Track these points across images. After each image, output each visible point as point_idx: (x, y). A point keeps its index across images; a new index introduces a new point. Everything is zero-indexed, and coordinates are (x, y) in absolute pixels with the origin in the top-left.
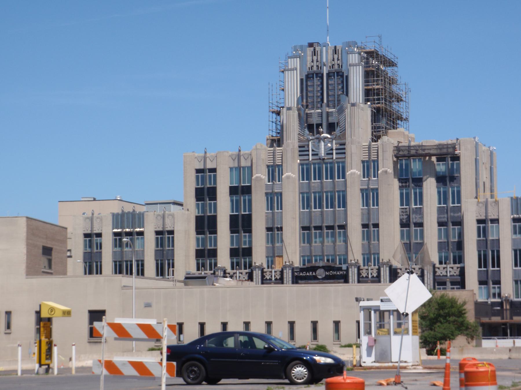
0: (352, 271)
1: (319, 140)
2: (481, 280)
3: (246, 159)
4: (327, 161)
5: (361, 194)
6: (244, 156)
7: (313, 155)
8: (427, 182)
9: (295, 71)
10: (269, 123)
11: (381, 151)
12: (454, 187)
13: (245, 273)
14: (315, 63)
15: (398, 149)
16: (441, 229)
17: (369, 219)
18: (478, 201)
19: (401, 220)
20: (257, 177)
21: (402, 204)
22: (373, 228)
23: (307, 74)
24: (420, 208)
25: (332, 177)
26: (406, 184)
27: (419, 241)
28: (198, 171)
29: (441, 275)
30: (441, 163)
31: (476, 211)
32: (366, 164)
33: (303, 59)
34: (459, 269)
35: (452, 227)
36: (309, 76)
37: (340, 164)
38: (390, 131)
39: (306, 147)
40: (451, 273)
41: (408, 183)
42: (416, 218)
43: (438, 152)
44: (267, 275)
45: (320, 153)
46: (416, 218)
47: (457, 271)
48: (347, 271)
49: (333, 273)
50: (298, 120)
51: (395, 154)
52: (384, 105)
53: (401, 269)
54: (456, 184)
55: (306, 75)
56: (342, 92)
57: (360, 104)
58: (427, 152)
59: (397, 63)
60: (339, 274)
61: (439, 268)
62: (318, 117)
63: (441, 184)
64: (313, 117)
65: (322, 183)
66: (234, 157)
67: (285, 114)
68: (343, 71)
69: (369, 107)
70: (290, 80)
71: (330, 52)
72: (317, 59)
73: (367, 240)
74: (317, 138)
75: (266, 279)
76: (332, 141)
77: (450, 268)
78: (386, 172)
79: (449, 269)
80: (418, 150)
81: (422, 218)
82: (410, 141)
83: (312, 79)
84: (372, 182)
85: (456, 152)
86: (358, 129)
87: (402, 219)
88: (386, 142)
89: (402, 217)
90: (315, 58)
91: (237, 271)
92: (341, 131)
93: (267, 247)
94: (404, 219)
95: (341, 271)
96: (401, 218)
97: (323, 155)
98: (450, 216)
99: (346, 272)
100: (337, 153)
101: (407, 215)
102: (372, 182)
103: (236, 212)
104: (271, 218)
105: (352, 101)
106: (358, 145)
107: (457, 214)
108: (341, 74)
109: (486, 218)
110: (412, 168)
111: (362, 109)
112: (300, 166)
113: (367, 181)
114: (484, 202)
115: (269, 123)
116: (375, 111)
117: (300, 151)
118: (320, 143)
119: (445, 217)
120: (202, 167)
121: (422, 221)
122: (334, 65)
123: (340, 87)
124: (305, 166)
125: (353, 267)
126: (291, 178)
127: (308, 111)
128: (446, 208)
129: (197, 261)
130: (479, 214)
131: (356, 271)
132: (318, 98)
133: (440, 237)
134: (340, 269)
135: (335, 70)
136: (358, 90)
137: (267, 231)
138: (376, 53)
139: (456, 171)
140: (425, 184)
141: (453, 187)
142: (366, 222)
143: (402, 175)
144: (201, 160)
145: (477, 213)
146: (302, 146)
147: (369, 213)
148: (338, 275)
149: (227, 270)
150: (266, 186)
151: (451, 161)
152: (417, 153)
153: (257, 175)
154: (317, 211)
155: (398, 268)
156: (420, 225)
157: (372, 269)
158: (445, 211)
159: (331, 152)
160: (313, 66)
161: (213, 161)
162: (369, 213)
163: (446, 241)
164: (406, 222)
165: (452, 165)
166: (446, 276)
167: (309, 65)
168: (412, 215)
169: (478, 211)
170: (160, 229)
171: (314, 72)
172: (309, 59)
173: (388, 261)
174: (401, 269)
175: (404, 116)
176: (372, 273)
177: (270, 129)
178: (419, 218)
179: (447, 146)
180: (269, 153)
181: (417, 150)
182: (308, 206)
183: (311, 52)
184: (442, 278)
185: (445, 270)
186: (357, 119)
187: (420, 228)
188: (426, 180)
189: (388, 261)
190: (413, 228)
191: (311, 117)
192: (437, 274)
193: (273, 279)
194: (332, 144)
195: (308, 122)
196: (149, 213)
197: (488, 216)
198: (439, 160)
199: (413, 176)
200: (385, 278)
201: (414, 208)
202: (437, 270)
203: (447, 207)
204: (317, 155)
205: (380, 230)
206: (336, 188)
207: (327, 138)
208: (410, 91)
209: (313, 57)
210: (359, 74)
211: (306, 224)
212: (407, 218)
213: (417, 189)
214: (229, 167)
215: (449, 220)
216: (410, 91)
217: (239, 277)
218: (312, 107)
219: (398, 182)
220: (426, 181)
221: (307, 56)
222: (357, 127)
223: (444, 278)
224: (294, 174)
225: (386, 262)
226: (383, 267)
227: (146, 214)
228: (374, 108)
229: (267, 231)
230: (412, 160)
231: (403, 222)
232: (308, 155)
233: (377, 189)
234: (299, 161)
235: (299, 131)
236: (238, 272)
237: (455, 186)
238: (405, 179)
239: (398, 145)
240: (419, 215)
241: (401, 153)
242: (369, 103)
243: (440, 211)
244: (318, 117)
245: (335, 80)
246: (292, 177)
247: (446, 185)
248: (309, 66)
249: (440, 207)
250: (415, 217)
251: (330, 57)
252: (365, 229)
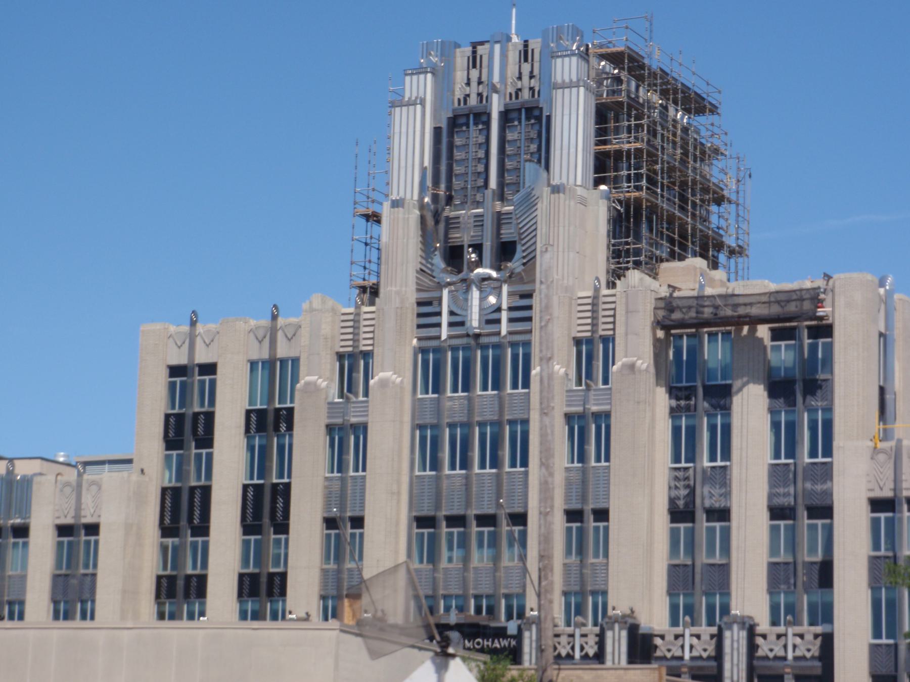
1: (467, 283)
2: (879, 673)
3: (290, 338)
4: (484, 340)
5: (567, 427)
6: (286, 331)
7: (451, 325)
8: (742, 395)
9: (419, 107)
10: (352, 246)
11: (624, 312)
12: (816, 410)
13: (708, 638)
14: (474, 89)
15: (668, 304)
16: (172, 455)
17: (584, 498)
18: (875, 448)
19: (672, 501)
20: (308, 384)
21: (676, 458)
22: (596, 520)
23: (451, 115)
24: (724, 468)
25: (498, 385)
26: (687, 402)
27: (718, 559)
28: (176, 371)
29: (771, 655)
30: (783, 344)
31: (868, 475)
32: (584, 347)
33: (443, 77)
34: (820, 639)
35: (806, 522)
36: (456, 123)
37: (519, 350)
38: (664, 265)
39: (435, 303)
40: (694, 650)
41: (693, 399)
42: (711, 496)
43: (775, 310)
44: (562, 644)
45: (469, 319)
46: (711, 496)
47: (814, 645)
48: (519, 637)
49: (483, 643)
50: (420, 233)
51: (659, 319)
52: (643, 194)
53: (662, 637)
54: (821, 401)
55: (449, 118)
56: (408, 101)
57: (577, 188)
58: (742, 311)
59: (717, 105)
60: (498, 646)
61: (764, 636)
62: (475, 226)
63: (782, 400)
64: (462, 226)
65: (470, 400)
66: (260, 334)
67: (387, 217)
68: (540, 106)
69: (602, 198)
70: (404, 130)
71: (513, 56)
72: (480, 78)
73: (489, 546)
74: (464, 280)
76: (500, 288)
77: (795, 635)
78: (632, 367)
79: (791, 640)
80: (720, 306)
81: (727, 495)
82: (702, 287)
83: (464, 128)
84: (595, 395)
85: (819, 310)
86: (566, 254)
87: (675, 498)
88: (634, 287)
89: (674, 493)
90: (474, 74)
91: (787, 630)
92: (525, 261)
93: (324, 572)
94: (679, 498)
95: (503, 639)
96: (673, 495)
97: (475, 323)
98: (804, 490)
99: (517, 643)
100: (511, 320)
101: (688, 486)
102: (595, 395)
103: (258, 479)
104: (339, 492)
105: (556, 181)
106: (564, 296)
107: (822, 486)
108: (536, 113)
109: (895, 496)
110: (706, 357)
111: (583, 202)
112: (420, 356)
113: (583, 393)
114: (891, 450)
115: (352, 246)
116: (622, 210)
117: (420, 315)
118: (470, 293)
119: (788, 494)
120: (183, 360)
121: (728, 505)
122: (520, 90)
123: (533, 147)
124: (431, 355)
125: (735, 627)
126: (391, 385)
127: (448, 212)
128: (792, 468)
129: (158, 608)
130: (876, 483)
132: (478, 177)
133: (774, 549)
134: (501, 633)
135: (523, 103)
136: (572, 150)
137: (328, 528)
138: (683, 92)
139: (823, 365)
140: (737, 401)
141: (812, 411)
142: (575, 506)
143: (679, 379)
144: (184, 343)
145: (869, 482)
146: (425, 300)
147: (584, 482)
148: (496, 648)
149: (758, 625)
150: (329, 408)
151: (809, 338)
152: (716, 314)
153: (308, 378)
154: (454, 476)
155: (656, 633)
156: (722, 514)
157: (584, 636)
158: (791, 476)
159: (495, 316)
160: (468, 95)
161: (210, 344)
162: (584, 482)
163: (790, 559)
164: (685, 508)
165: (813, 349)
166: (785, 658)
167: (458, 94)
168: (702, 487)
169: (875, 476)
170: (69, 520)
171: (471, 109)
172: (460, 76)
173: (628, 612)
174: (662, 637)
175: (730, 241)
177: (355, 259)
178: (721, 495)
179: (797, 296)
180: (343, 321)
181: (717, 307)
182: (436, 465)
183: (466, 58)
184: (771, 663)
186: (564, 227)
187: (723, 524)
188: (740, 390)
189: (628, 612)
190: (703, 523)
191: (458, 227)
192: (760, 653)
193: (577, 655)
194: (499, 296)
195: (450, 241)
196: (43, 478)
197: (901, 490)
198: (777, 335)
199: (708, 381)
201: (708, 467)
202: (759, 641)
203: (795, 464)
204: (462, 324)
205: (611, 528)
206: (506, 413)
207: (488, 278)
208: (750, 176)
209: (470, 72)
210: (576, 107)
211: (426, 512)
212: (688, 495)
213: (716, 415)
214: (249, 361)
215: (800, 500)
216: (750, 176)
217: (692, 647)
218: (462, 203)
219: (667, 396)
220: (740, 394)
221: (454, 70)
222: (564, 249)
223: (780, 664)
224: (399, 376)
225: (620, 614)
226: (612, 629)
227: (37, 479)
228: (620, 202)
229: (328, 528)
230: (706, 336)
231: (678, 507)
232: (439, 325)
233: (608, 415)
234: (415, 341)
235: (421, 263)
236: (790, 631)
237: (817, 406)
238: (686, 388)
239: (671, 295)
240: (720, 488)
241: (677, 316)
242: (603, 187)
243: (777, 475)
244: (475, 226)
245: (521, 129)
246: (394, 383)
247: (794, 404)
248: (459, 97)
249: (778, 465)
250: (710, 492)
251: (512, 70)
252: (575, 525)
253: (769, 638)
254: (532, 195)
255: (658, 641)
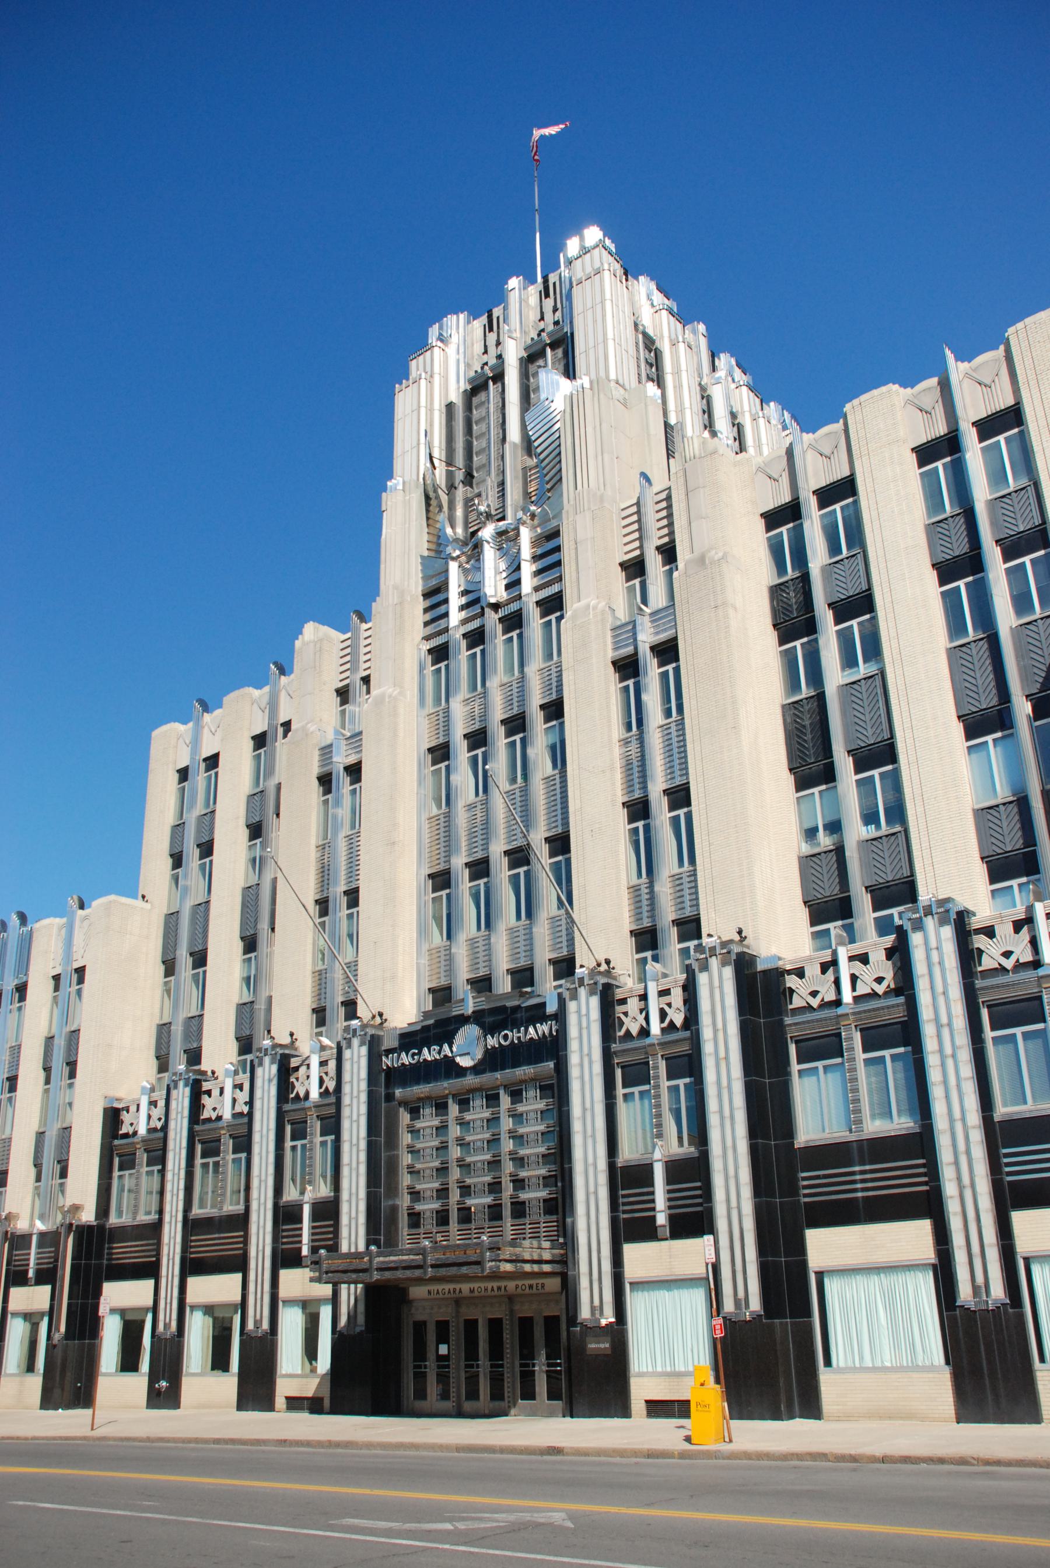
0: (579, 1011)
13: (882, 955)
29: (815, 1002)
40: (859, 983)
53: (800, 973)
61: (989, 932)
75: (628, 1033)
95: (542, 1024)
131: (595, 1014)
149: (974, 914)
174: (800, 973)
176: (666, 1008)
185: (830, 975)
192: (987, 963)
193: (655, 1028)
200: (720, 1025)
202: (980, 941)
217: (854, 979)
253: (872, 958)
254: (552, 410)
255: (791, 981)
